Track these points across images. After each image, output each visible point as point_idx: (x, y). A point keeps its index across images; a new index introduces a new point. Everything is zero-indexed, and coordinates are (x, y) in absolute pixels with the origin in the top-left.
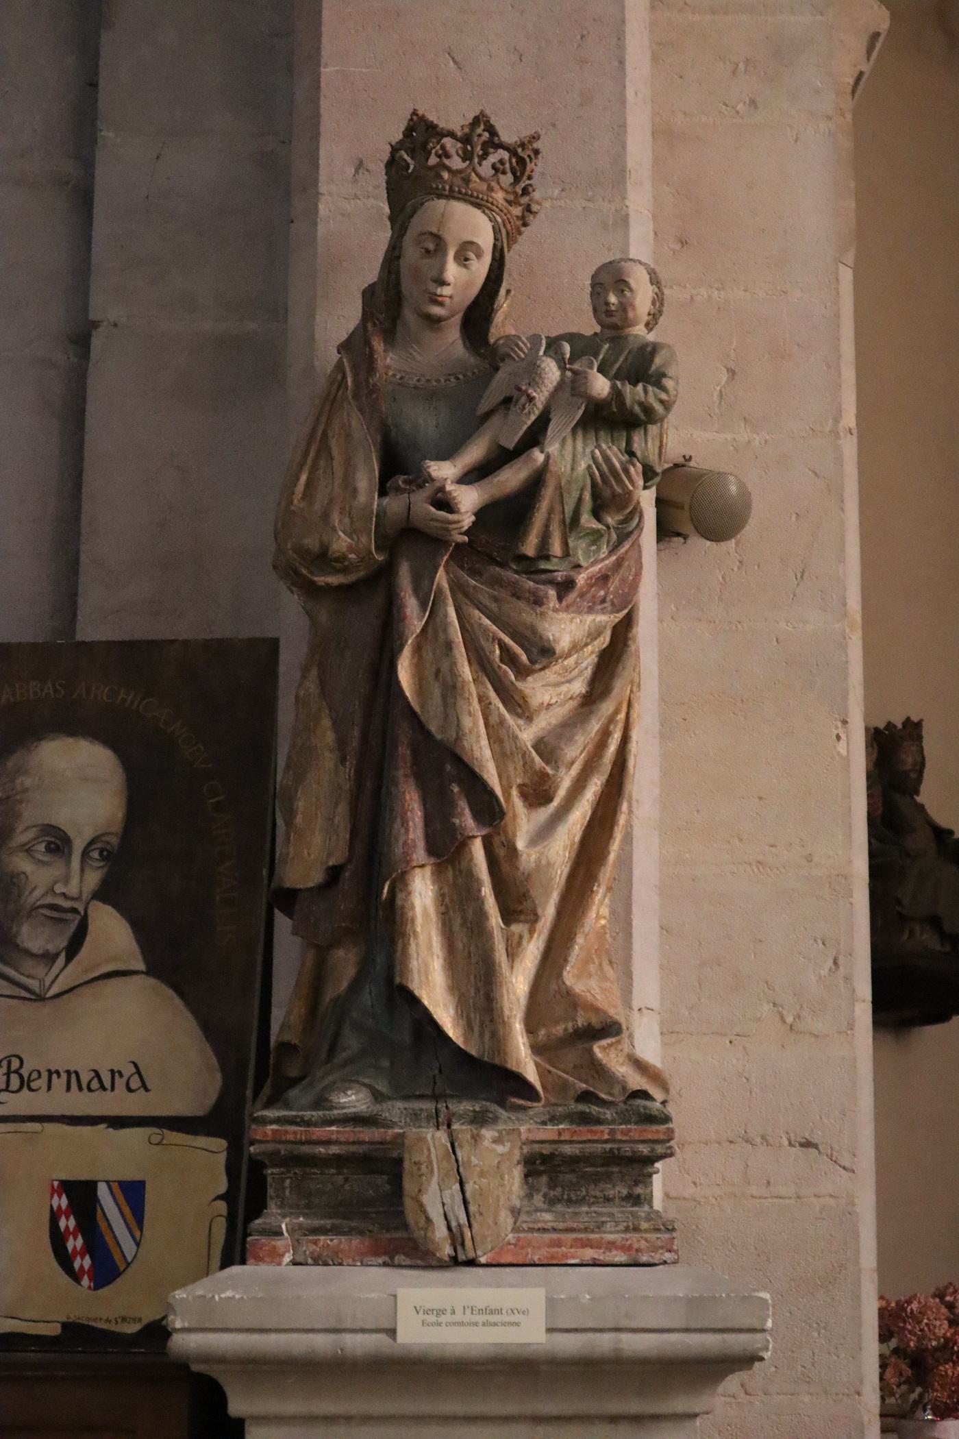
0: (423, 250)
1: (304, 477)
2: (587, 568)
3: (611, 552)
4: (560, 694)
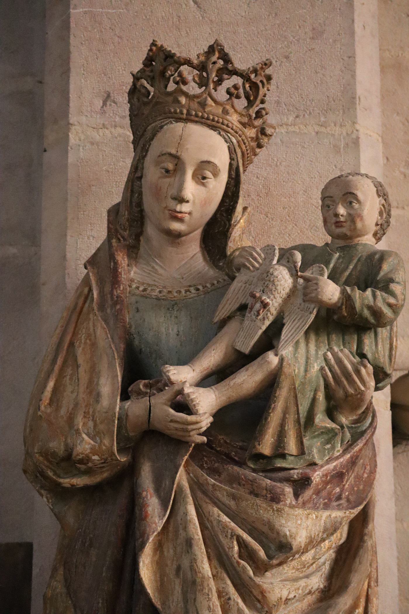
0: (163, 171)
1: (51, 384)
2: (322, 466)
3: (345, 451)
4: (299, 589)
